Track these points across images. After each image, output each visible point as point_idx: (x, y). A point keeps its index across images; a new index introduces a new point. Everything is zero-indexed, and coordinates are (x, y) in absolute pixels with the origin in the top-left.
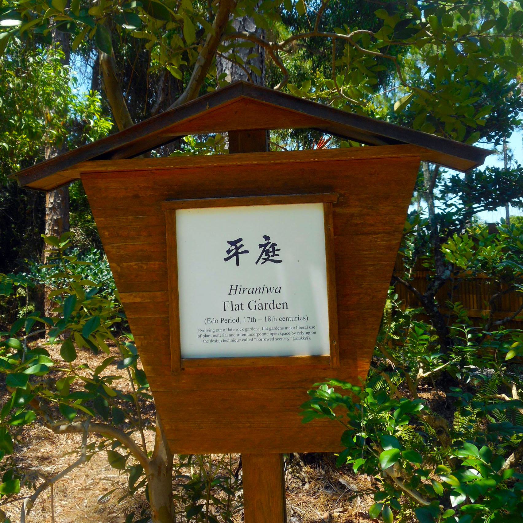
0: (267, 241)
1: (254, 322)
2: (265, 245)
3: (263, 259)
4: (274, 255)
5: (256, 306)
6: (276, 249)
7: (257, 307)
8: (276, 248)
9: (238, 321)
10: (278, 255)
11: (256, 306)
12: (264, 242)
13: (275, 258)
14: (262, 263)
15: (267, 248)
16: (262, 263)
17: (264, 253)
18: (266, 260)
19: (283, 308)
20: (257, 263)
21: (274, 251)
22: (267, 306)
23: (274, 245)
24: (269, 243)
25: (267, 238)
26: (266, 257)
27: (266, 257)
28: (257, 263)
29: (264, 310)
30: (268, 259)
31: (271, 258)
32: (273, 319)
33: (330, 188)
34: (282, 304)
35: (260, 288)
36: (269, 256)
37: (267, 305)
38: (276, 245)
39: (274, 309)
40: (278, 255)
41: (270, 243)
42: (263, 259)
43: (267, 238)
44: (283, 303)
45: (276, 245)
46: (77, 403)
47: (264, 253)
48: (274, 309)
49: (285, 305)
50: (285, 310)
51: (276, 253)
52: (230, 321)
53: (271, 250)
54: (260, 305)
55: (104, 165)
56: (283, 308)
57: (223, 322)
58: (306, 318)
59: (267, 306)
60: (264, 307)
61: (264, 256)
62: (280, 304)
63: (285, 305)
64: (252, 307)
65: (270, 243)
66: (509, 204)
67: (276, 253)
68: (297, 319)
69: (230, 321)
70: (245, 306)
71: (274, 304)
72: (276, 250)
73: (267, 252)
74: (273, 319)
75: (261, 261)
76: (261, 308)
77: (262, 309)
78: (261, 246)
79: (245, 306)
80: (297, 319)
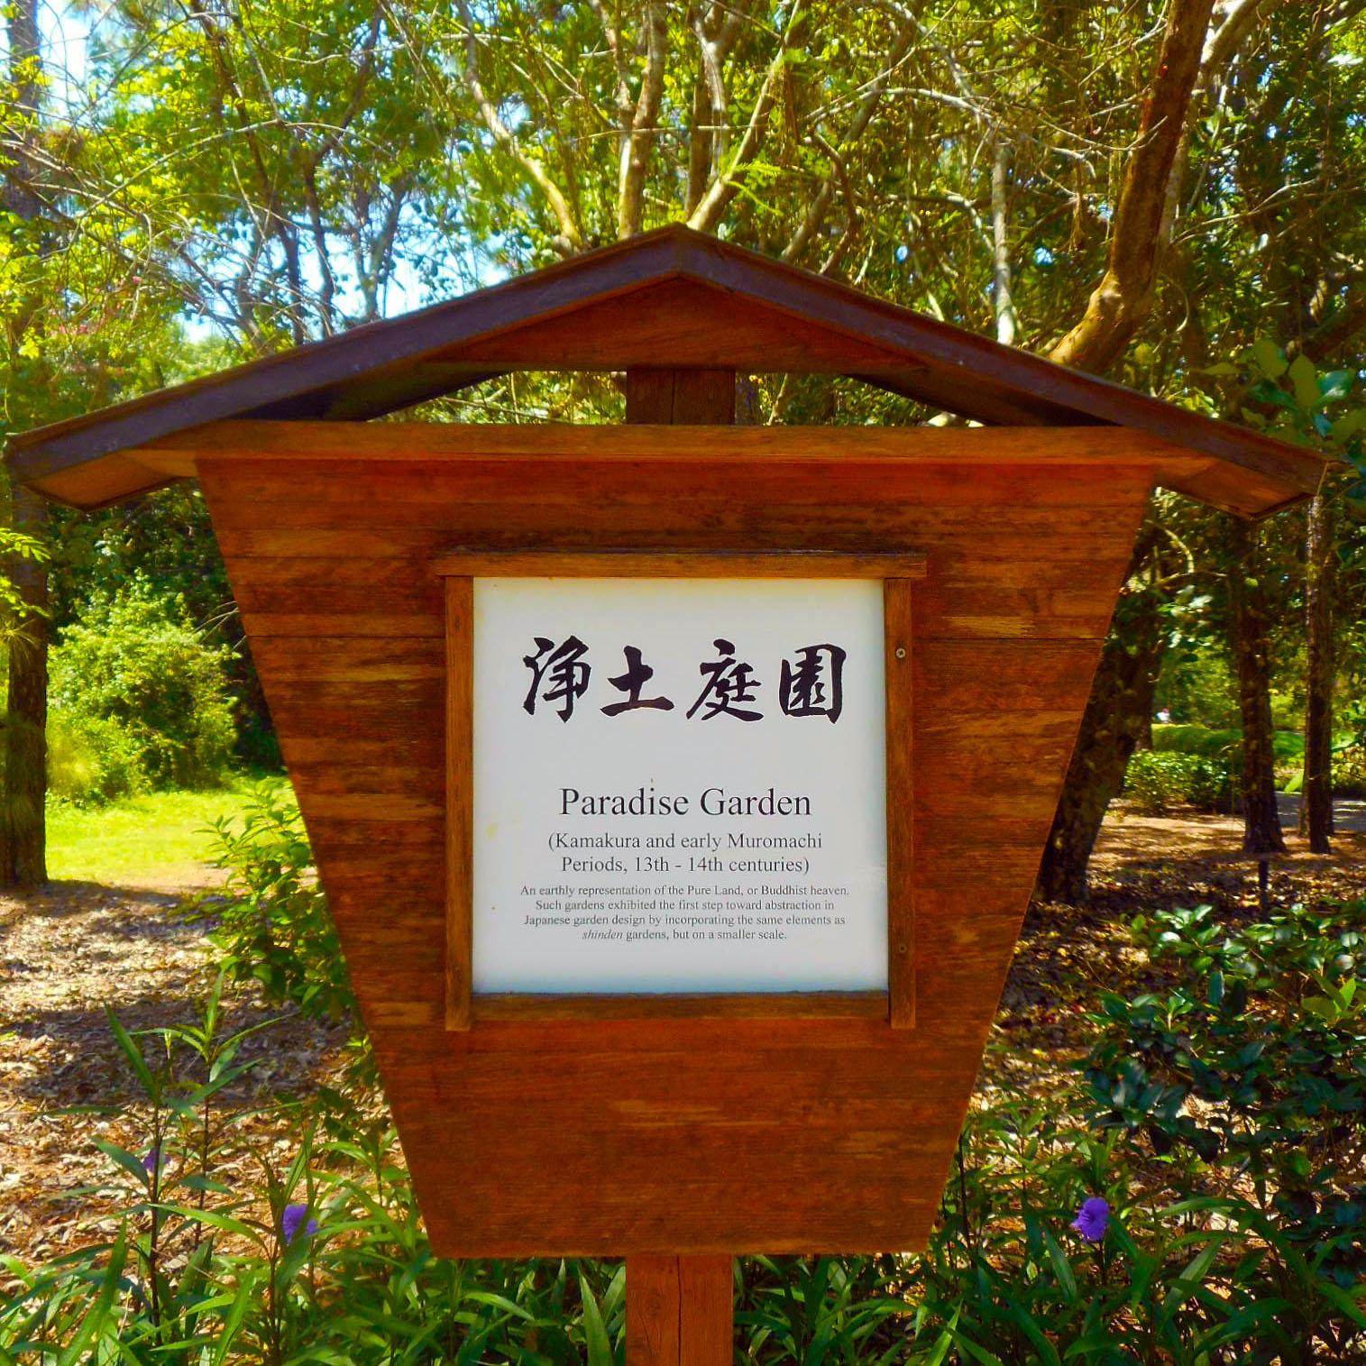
0: (725, 657)
1: (664, 872)
2: (719, 668)
3: (709, 705)
4: (740, 698)
5: (722, 803)
6: (748, 680)
8: (749, 677)
10: (751, 698)
11: (722, 803)
12: (716, 657)
13: (743, 706)
14: (706, 717)
15: (724, 675)
16: (706, 717)
17: (714, 689)
18: (718, 708)
20: (690, 714)
21: (742, 684)
22: (754, 805)
23: (745, 668)
24: (729, 662)
25: (725, 647)
26: (719, 701)
27: (719, 701)
28: (690, 714)
29: (744, 816)
31: (731, 704)
36: (726, 698)
37: (752, 802)
38: (750, 669)
39: (772, 813)
40: (751, 698)
41: (734, 661)
42: (709, 705)
43: (725, 647)
44: (798, 800)
45: (750, 669)
47: (714, 689)
48: (772, 813)
49: (803, 804)
50: (803, 817)
51: (748, 691)
52: (588, 866)
53: (733, 681)
55: (871, 454)
57: (569, 867)
59: (754, 805)
60: (744, 808)
61: (712, 697)
63: (803, 804)
64: (712, 804)
65: (734, 661)
66: (1118, 295)
67: (748, 691)
68: (779, 866)
69: (588, 866)
71: (772, 800)
72: (749, 684)
73: (723, 687)
75: (704, 710)
76: (735, 809)
78: (705, 668)
80: (779, 866)
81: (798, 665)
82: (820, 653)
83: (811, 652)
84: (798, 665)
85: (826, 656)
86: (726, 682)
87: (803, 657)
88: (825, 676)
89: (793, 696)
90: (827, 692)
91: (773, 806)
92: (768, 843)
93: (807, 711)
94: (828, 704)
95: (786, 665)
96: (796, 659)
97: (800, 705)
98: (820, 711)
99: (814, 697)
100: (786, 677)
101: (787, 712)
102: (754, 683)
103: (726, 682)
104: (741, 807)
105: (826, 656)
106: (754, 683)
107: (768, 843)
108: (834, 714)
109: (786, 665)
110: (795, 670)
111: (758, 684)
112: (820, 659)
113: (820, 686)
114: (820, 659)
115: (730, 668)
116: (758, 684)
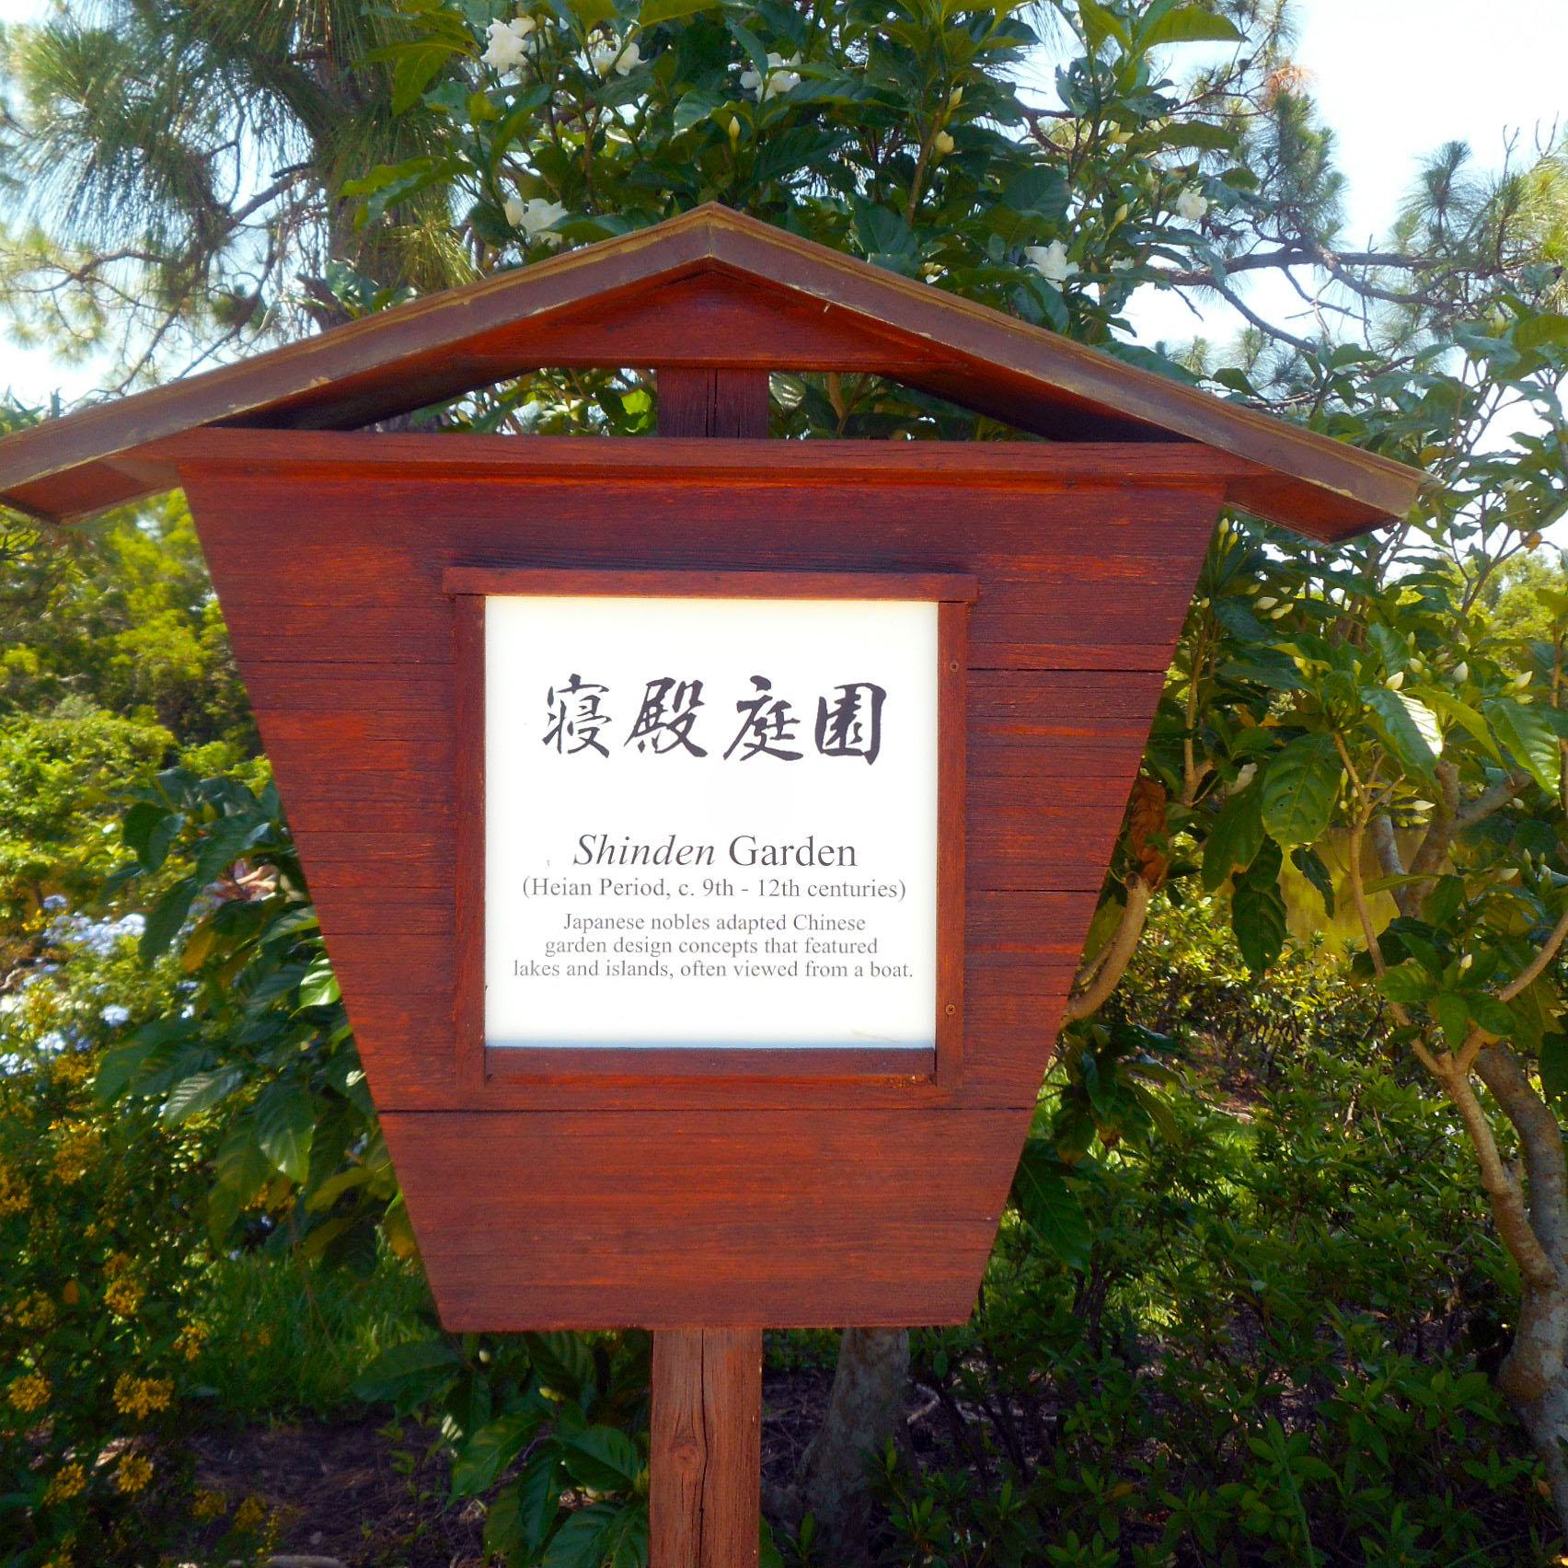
0: (762, 693)
1: (794, 899)
2: (755, 706)
3: (746, 745)
4: (779, 737)
6: (786, 718)
7: (759, 856)
8: (787, 714)
9: (659, 891)
10: (791, 737)
12: (753, 694)
15: (762, 713)
18: (757, 748)
19: (841, 864)
20: (726, 755)
21: (781, 723)
22: (791, 855)
23: (780, 707)
24: (766, 699)
26: (757, 741)
27: (757, 741)
28: (726, 755)
30: (761, 747)
31: (769, 744)
32: (721, 889)
33: (956, 567)
34: (837, 852)
35: (647, 848)
37: (789, 851)
38: (787, 706)
40: (791, 737)
41: (771, 698)
42: (746, 745)
43: (762, 683)
44: (841, 849)
45: (787, 706)
46: (1113, 51)
47: (752, 728)
48: (811, 863)
49: (847, 854)
51: (787, 729)
52: (632, 890)
53: (772, 719)
54: (769, 850)
56: (841, 864)
57: (609, 891)
58: (900, 891)
59: (791, 855)
60: (779, 858)
61: (750, 736)
62: (832, 851)
63: (847, 854)
64: (742, 853)
65: (771, 698)
67: (787, 729)
68: (869, 891)
69: (632, 890)
70: (722, 853)
71: (811, 849)
74: (721, 889)
75: (741, 750)
76: (769, 859)
77: (774, 863)
78: (742, 706)
79: (722, 853)
80: (869, 891)
81: (837, 702)
82: (859, 691)
83: (850, 689)
84: (837, 702)
85: (866, 696)
86: (763, 720)
87: (842, 694)
88: (864, 714)
89: (829, 734)
90: (866, 732)
91: (813, 855)
92: (825, 971)
93: (844, 751)
94: (865, 746)
95: (822, 702)
96: (834, 699)
97: (836, 745)
98: (857, 753)
99: (850, 735)
100: (823, 715)
101: (822, 751)
102: (794, 721)
103: (763, 720)
104: (774, 856)
105: (866, 696)
106: (794, 721)
107: (825, 971)
108: (871, 756)
109: (822, 702)
110: (832, 707)
111: (798, 722)
112: (859, 697)
113: (858, 726)
114: (859, 697)
115: (768, 706)
116: (798, 722)
